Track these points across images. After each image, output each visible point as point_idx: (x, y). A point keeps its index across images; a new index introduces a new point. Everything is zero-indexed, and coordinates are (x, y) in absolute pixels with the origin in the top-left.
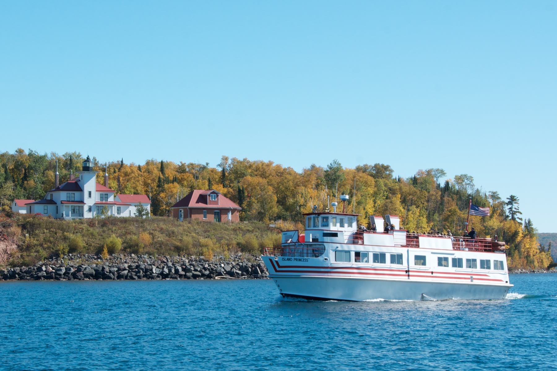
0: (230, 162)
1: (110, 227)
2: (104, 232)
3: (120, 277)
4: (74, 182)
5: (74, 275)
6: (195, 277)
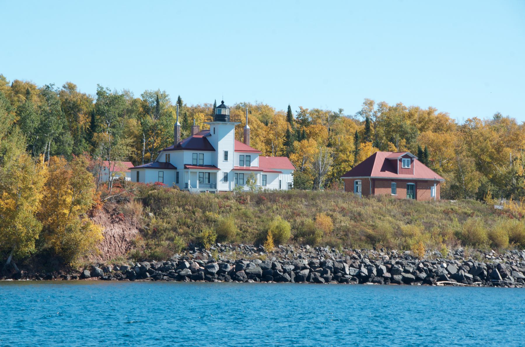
0: (376, 108)
1: (269, 204)
2: (261, 211)
3: (299, 279)
4: (201, 136)
5: (234, 275)
6: (407, 281)
